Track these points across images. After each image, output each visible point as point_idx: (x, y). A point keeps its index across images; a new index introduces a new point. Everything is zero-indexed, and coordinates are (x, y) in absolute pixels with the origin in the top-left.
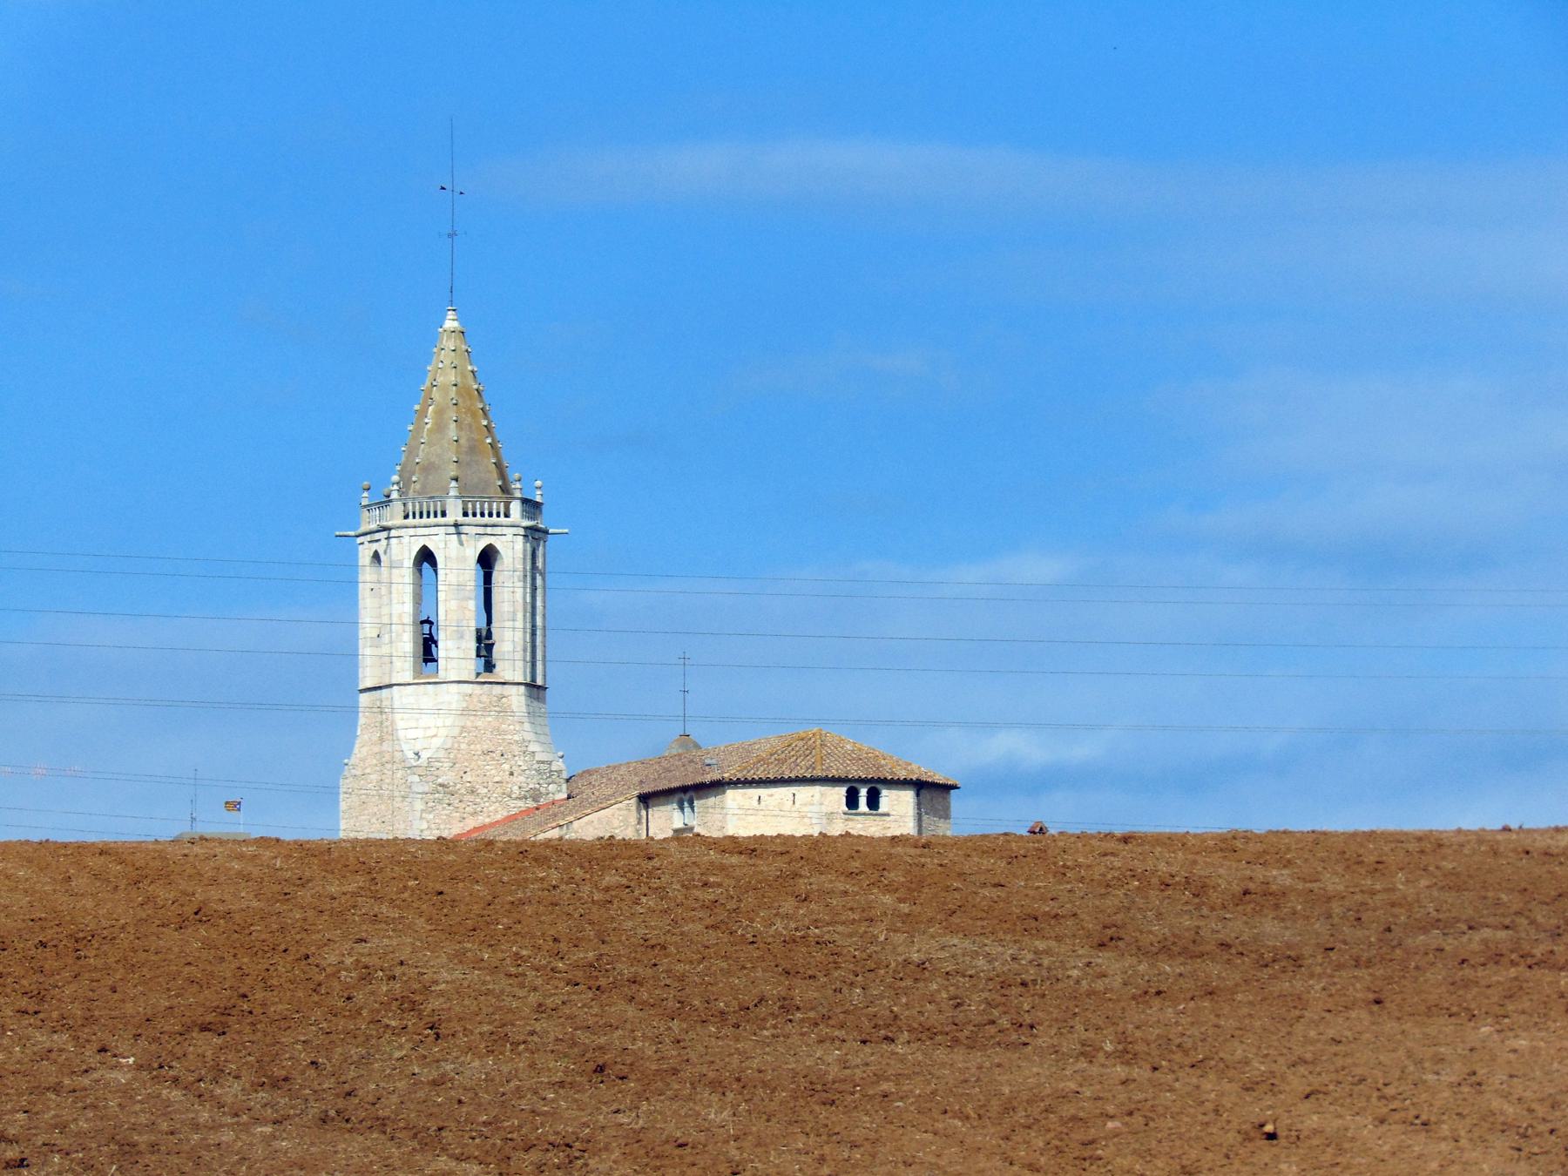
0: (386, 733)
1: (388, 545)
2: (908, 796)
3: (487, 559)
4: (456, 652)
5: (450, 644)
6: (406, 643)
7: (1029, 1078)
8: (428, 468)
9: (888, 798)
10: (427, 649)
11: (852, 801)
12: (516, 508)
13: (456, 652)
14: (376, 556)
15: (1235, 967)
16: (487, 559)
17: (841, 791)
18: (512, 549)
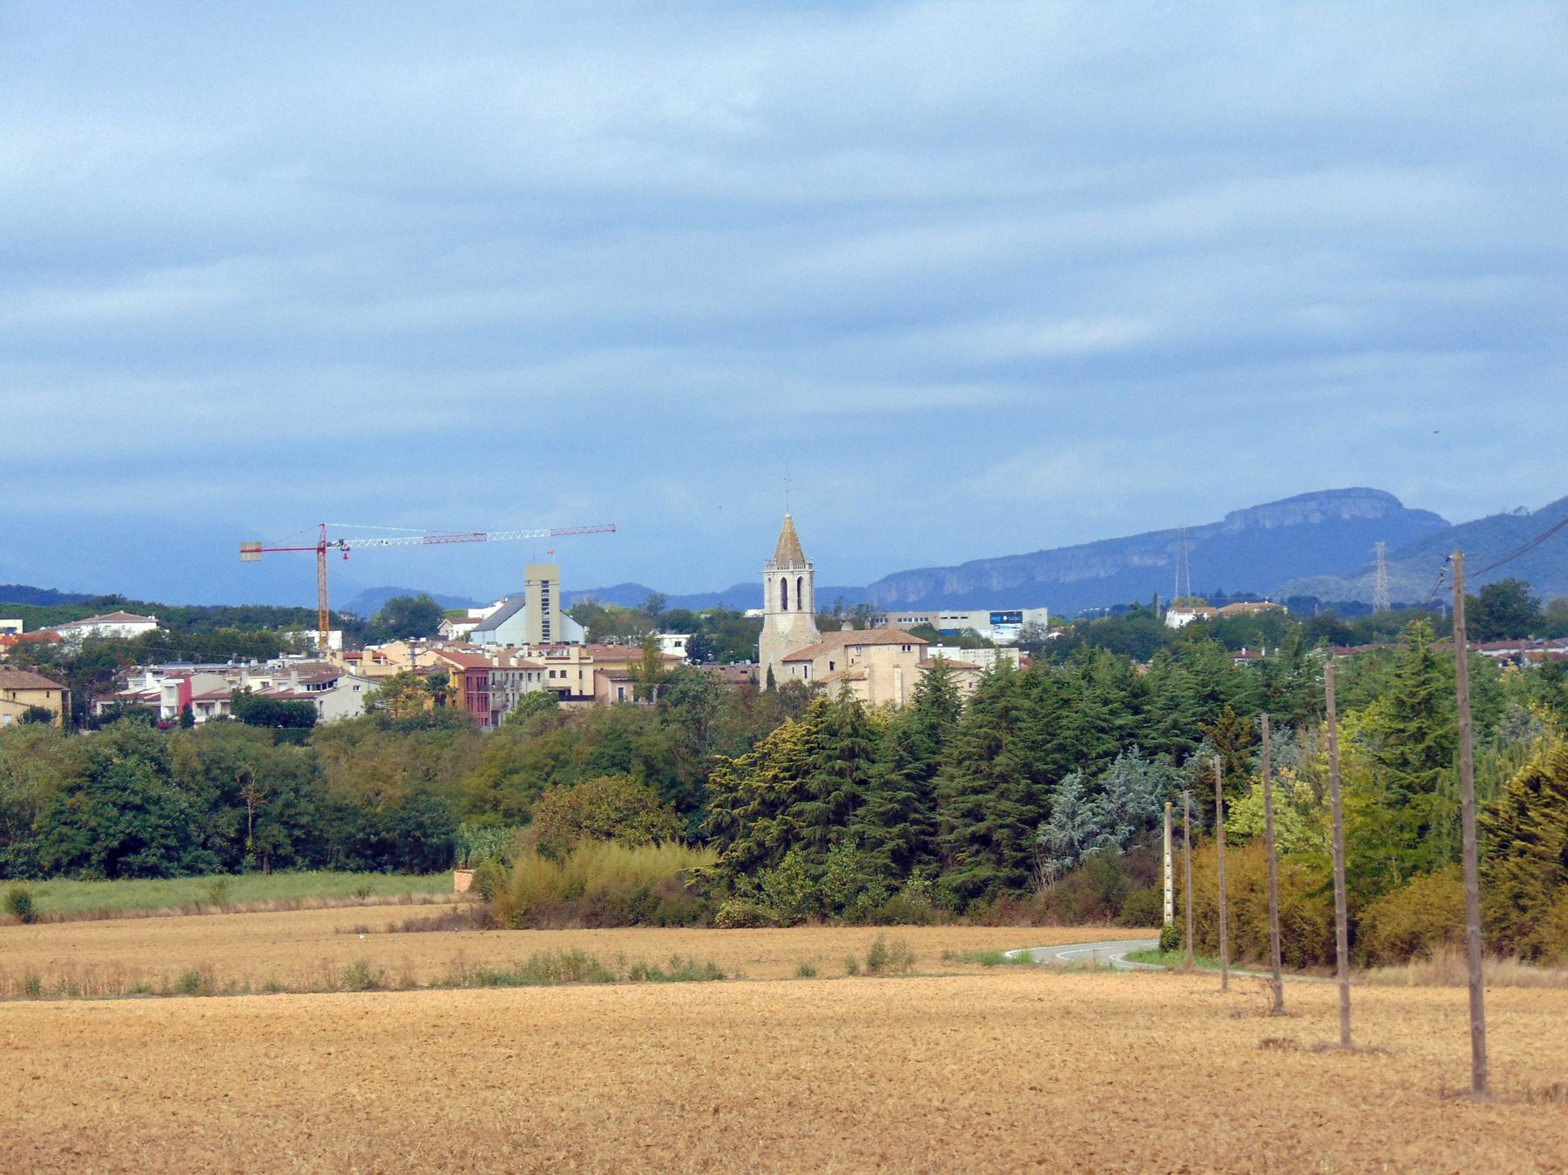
0: (774, 626)
1: (1458, 1094)
2: (918, 647)
3: (799, 581)
4: (792, 605)
5: (1272, 930)
6: (779, 603)
7: (1274, 1110)
8: (783, 556)
9: (912, 648)
10: (785, 607)
11: (904, 649)
12: (807, 566)
13: (792, 605)
14: (770, 579)
15: (605, 896)
16: (799, 581)
17: (901, 647)
18: (806, 578)
